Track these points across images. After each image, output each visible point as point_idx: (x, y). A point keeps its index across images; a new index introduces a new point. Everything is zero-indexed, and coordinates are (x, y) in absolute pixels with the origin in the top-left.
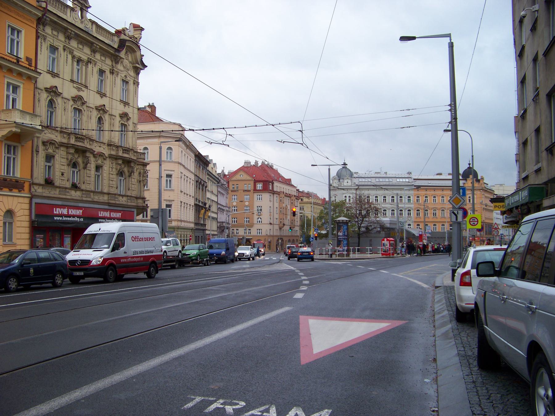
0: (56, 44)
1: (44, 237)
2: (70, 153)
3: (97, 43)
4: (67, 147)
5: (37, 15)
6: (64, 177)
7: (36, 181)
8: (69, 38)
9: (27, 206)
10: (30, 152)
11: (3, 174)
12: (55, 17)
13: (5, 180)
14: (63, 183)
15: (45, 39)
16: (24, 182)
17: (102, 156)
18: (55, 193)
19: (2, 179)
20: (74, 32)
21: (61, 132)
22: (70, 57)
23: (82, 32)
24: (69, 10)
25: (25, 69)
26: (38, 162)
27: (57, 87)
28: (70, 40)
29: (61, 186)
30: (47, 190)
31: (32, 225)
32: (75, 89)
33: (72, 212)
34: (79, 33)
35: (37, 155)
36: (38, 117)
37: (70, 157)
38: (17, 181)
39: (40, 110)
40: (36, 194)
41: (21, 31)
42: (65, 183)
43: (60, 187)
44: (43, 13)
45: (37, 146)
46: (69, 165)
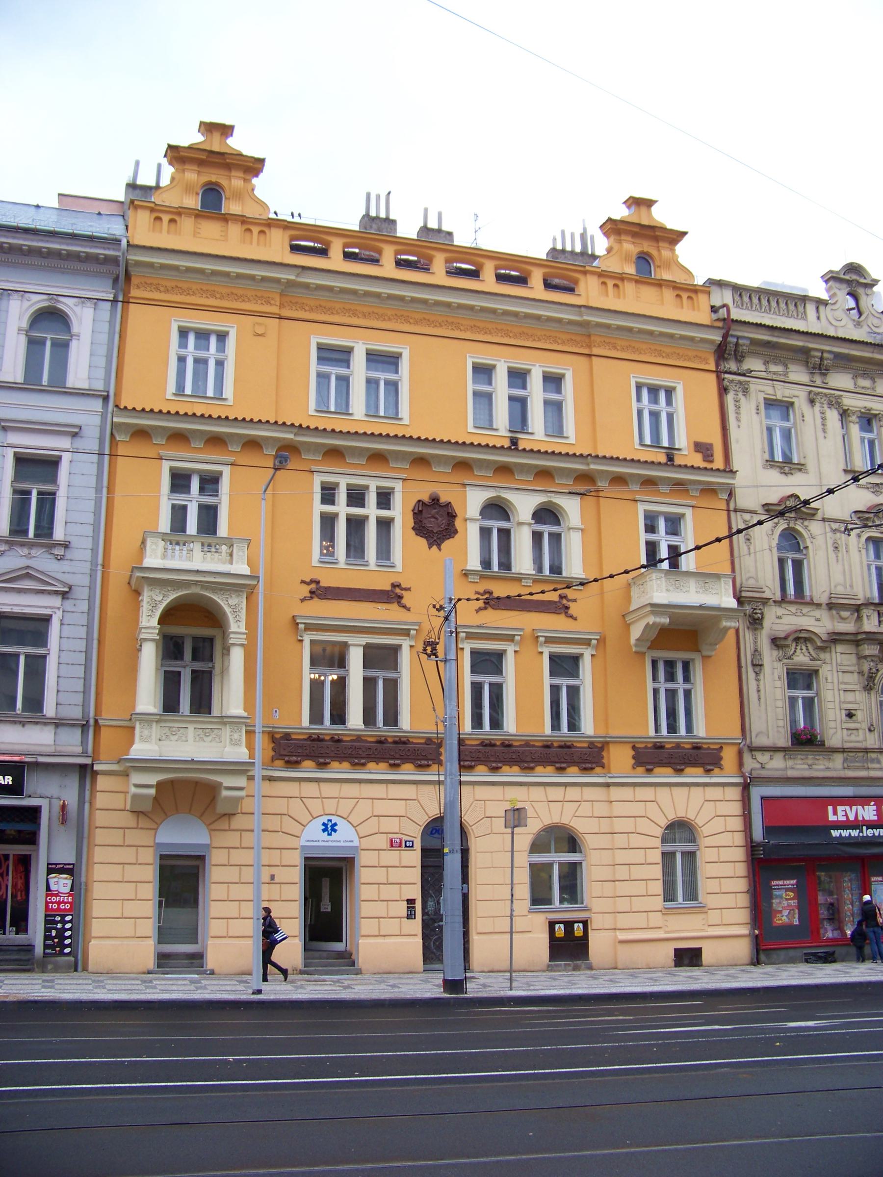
0: (782, 392)
1: (797, 882)
2: (865, 657)
4: (857, 643)
5: (712, 342)
6: (855, 722)
8: (820, 368)
9: (736, 808)
11: (652, 732)
13: (659, 747)
14: (853, 738)
15: (746, 392)
16: (721, 747)
17: (806, 640)
18: (836, 765)
19: (649, 745)
20: (830, 352)
21: (831, 606)
22: (833, 416)
24: (811, 308)
25: (684, 470)
26: (762, 692)
28: (825, 375)
29: (846, 745)
30: (800, 762)
31: (752, 855)
32: (866, 491)
34: (846, 351)
35: (757, 674)
36: (722, 580)
37: (866, 666)
38: (697, 747)
39: (756, 561)
40: (764, 773)
41: (674, 388)
42: (861, 738)
43: (843, 750)
44: (723, 331)
45: (756, 652)
46: (871, 689)
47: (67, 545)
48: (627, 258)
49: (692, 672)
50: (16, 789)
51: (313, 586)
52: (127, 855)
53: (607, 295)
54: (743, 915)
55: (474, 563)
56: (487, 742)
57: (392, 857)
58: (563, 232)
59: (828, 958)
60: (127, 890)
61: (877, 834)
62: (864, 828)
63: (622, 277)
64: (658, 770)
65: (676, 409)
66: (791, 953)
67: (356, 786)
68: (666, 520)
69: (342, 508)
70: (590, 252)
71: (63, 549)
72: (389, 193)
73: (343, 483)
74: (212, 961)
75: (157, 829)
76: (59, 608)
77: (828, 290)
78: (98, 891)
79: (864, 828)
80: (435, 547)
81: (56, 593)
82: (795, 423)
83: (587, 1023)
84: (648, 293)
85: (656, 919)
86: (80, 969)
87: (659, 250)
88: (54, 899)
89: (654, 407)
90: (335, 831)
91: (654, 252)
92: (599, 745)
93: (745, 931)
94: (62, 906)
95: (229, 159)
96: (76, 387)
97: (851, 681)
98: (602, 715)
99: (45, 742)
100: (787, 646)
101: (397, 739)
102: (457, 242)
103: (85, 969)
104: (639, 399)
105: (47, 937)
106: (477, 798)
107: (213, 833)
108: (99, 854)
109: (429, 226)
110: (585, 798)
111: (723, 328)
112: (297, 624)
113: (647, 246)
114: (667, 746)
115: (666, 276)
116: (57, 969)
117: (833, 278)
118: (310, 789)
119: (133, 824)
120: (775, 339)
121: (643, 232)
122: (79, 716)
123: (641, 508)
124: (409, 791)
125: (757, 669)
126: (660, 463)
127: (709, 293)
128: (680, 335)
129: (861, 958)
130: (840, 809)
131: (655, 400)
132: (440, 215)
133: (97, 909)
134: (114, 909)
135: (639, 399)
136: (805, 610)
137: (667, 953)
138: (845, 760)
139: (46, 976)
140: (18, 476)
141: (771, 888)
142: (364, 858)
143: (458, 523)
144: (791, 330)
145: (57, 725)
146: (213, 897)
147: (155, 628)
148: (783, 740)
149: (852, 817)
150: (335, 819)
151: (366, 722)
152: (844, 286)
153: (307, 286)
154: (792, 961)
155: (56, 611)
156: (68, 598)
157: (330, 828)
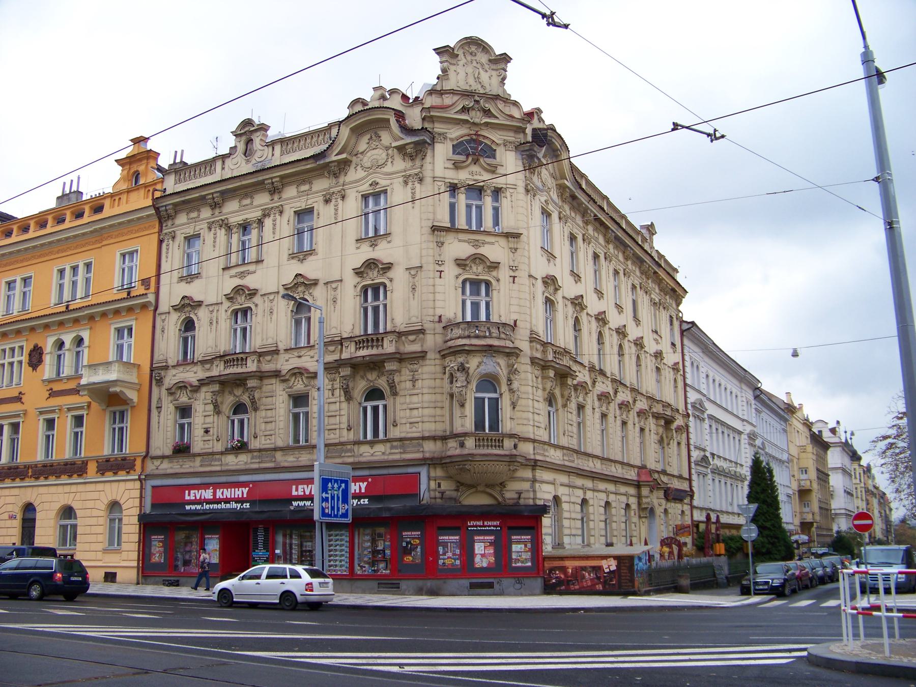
3: (267, 177)
7: (154, 452)
9: (137, 493)
10: (146, 411)
12: (217, 186)
18: (195, 465)
23: (286, 167)
27: (300, 275)
30: (176, 464)
33: (222, 493)
38: (124, 459)
43: (199, 455)
51: (50, 391)
54: (134, 555)
57: (9, 523)
61: (211, 508)
62: (205, 504)
66: (157, 579)
67: (55, 487)
79: (205, 504)
85: (100, 555)
120: (183, 199)
121: (132, 160)
123: (113, 327)
124: (15, 491)
125: (159, 409)
126: (63, 312)
130: (300, 487)
136: (188, 368)
138: (201, 461)
141: (151, 539)
144: (188, 190)
149: (307, 493)
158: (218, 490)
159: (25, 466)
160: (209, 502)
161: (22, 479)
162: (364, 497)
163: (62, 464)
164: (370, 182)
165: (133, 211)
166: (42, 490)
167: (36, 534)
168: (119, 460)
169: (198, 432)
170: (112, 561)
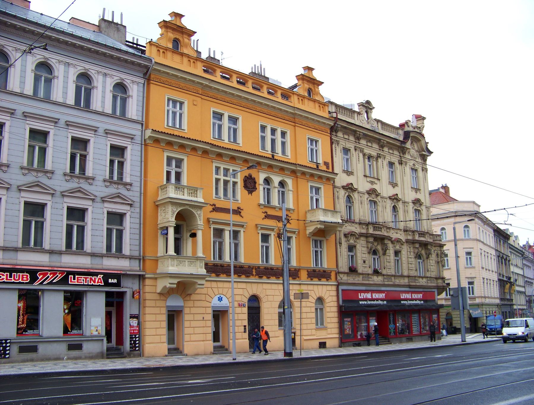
2: (370, 242)
5: (330, 125)
7: (341, 270)
9: (335, 293)
14: (365, 270)
15: (338, 144)
16: (331, 272)
17: (354, 235)
19: (312, 270)
20: (362, 133)
21: (360, 224)
22: (361, 155)
26: (341, 253)
29: (364, 272)
30: (351, 278)
33: (375, 296)
35: (340, 246)
37: (416, 251)
38: (324, 271)
42: (367, 270)
43: (362, 274)
47: (9, 166)
48: (169, 40)
49: (182, 230)
50: (118, 285)
52: (157, 310)
53: (160, 56)
54: (336, 331)
55: (262, 201)
56: (216, 264)
58: (255, 65)
59: (359, 345)
60: (157, 325)
63: (166, 49)
64: (314, 279)
65: (318, 149)
66: (350, 343)
68: (315, 189)
69: (222, 178)
70: (263, 75)
71: (6, 167)
72: (198, 40)
73: (222, 167)
74: (186, 351)
75: (166, 300)
76: (129, 211)
77: (359, 109)
78: (148, 325)
80: (250, 194)
81: (128, 204)
82: (350, 157)
83: (216, 378)
84: (177, 58)
85: (314, 332)
86: (142, 356)
87: (314, 88)
88: (132, 329)
89: (174, 110)
90: (222, 300)
91: (181, 39)
92: (252, 267)
93: (337, 336)
94: (135, 331)
95: (184, 30)
96: (132, 118)
97: (364, 250)
98: (299, 260)
99: (125, 265)
100: (395, 243)
101: (240, 266)
102: (270, 82)
103: (143, 356)
104: (168, 105)
105: (131, 344)
106: (264, 288)
107: (185, 301)
108: (148, 310)
109: (106, 18)
110: (294, 289)
111: (334, 121)
112: (210, 221)
113: (311, 86)
114: (275, 269)
115: (185, 51)
116: (134, 356)
117: (362, 105)
118: (214, 285)
119: (158, 298)
120: (348, 126)
122: (138, 255)
123: (166, 154)
124: (243, 285)
126: (269, 158)
127: (328, 106)
128: (163, 71)
129: (369, 345)
131: (175, 107)
132: (214, 52)
133: (147, 332)
134: (153, 332)
135: (168, 105)
137: (316, 343)
139: (130, 359)
140: (73, 147)
142: (230, 311)
143: (257, 185)
145: (130, 259)
146: (186, 326)
147: (174, 222)
148: (347, 270)
150: (222, 296)
151: (107, 251)
152: (365, 108)
153: (211, 87)
154: (349, 346)
155: (128, 212)
156: (132, 207)
157: (220, 299)
158: (373, 294)
159: (249, 267)
160: (370, 300)
161: (247, 277)
162: (422, 300)
163: (238, 266)
164: (105, 72)
165: (164, 65)
166: (265, 286)
167: (247, 320)
168: (321, 272)
169: (360, 262)
170: (322, 335)
